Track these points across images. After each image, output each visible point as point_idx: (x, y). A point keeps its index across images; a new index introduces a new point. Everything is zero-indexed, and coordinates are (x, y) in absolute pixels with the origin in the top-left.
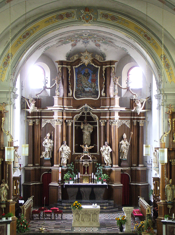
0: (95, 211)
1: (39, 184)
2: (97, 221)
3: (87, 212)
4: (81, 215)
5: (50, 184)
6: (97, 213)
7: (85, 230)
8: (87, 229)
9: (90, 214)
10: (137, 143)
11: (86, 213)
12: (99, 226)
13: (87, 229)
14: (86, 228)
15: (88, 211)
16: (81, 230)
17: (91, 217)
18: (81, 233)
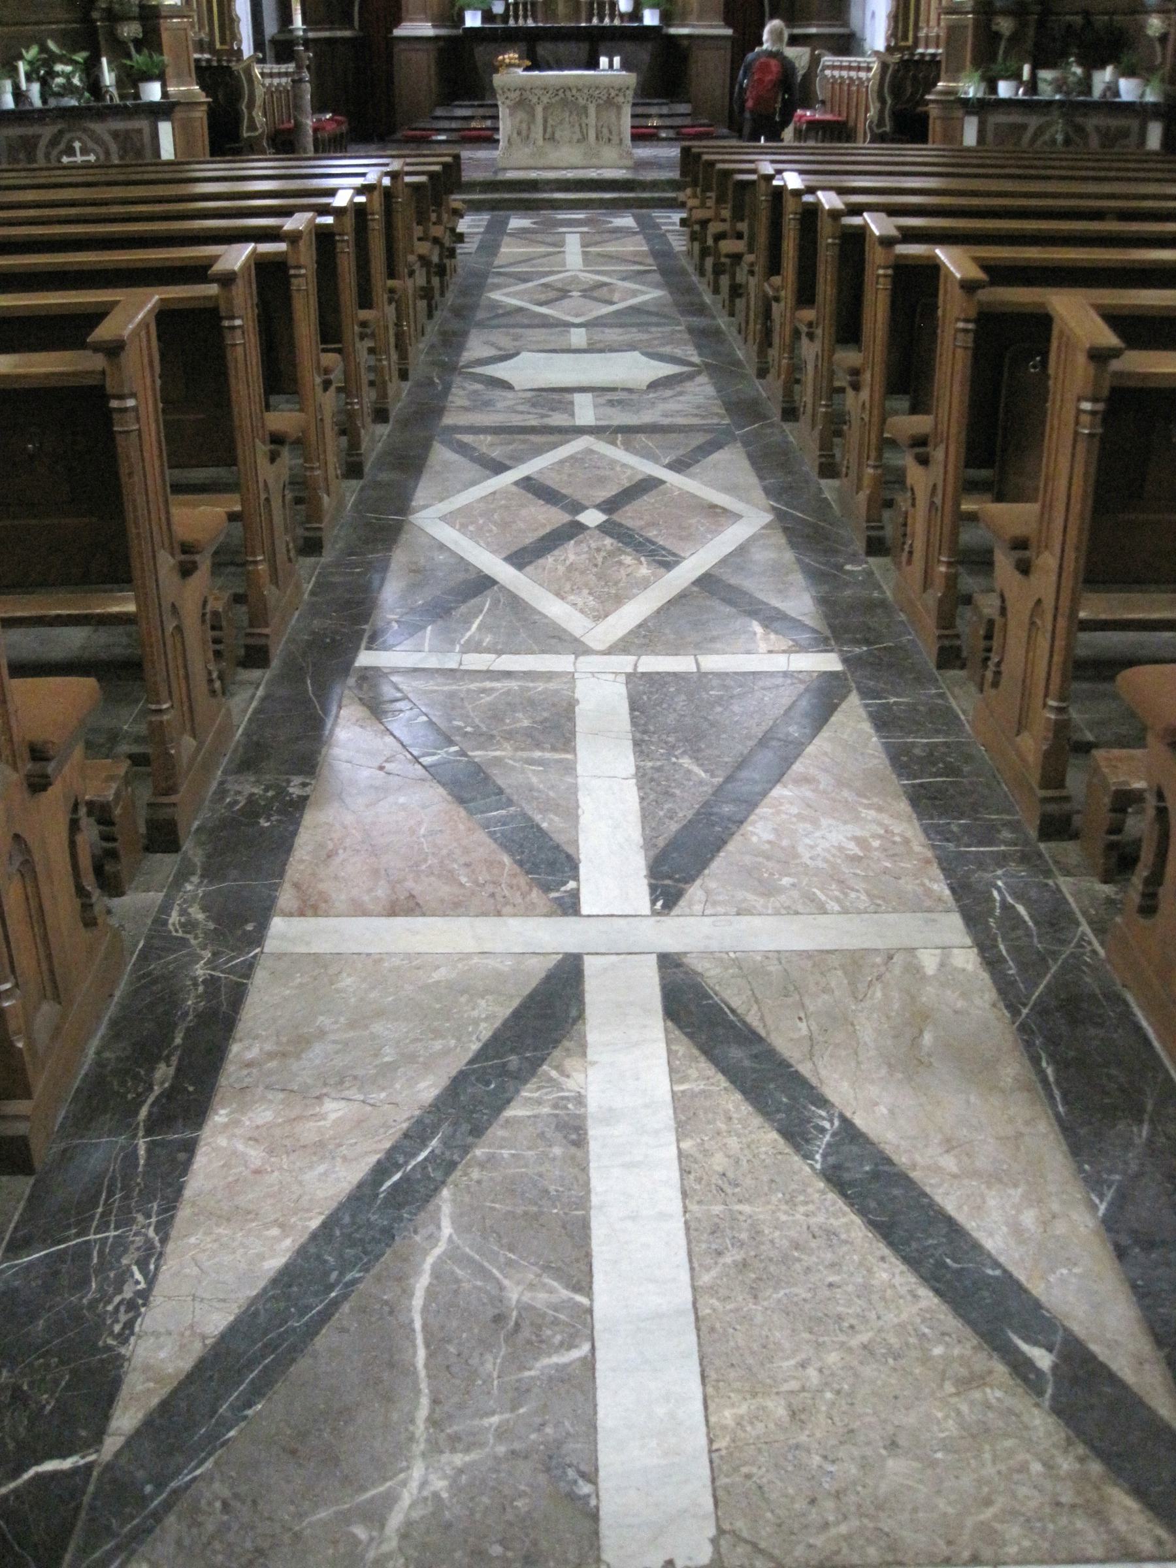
1: (344, 40)
3: (568, 93)
4: (539, 110)
5: (398, 32)
6: (621, 99)
9: (585, 108)
11: (564, 103)
17: (592, 119)
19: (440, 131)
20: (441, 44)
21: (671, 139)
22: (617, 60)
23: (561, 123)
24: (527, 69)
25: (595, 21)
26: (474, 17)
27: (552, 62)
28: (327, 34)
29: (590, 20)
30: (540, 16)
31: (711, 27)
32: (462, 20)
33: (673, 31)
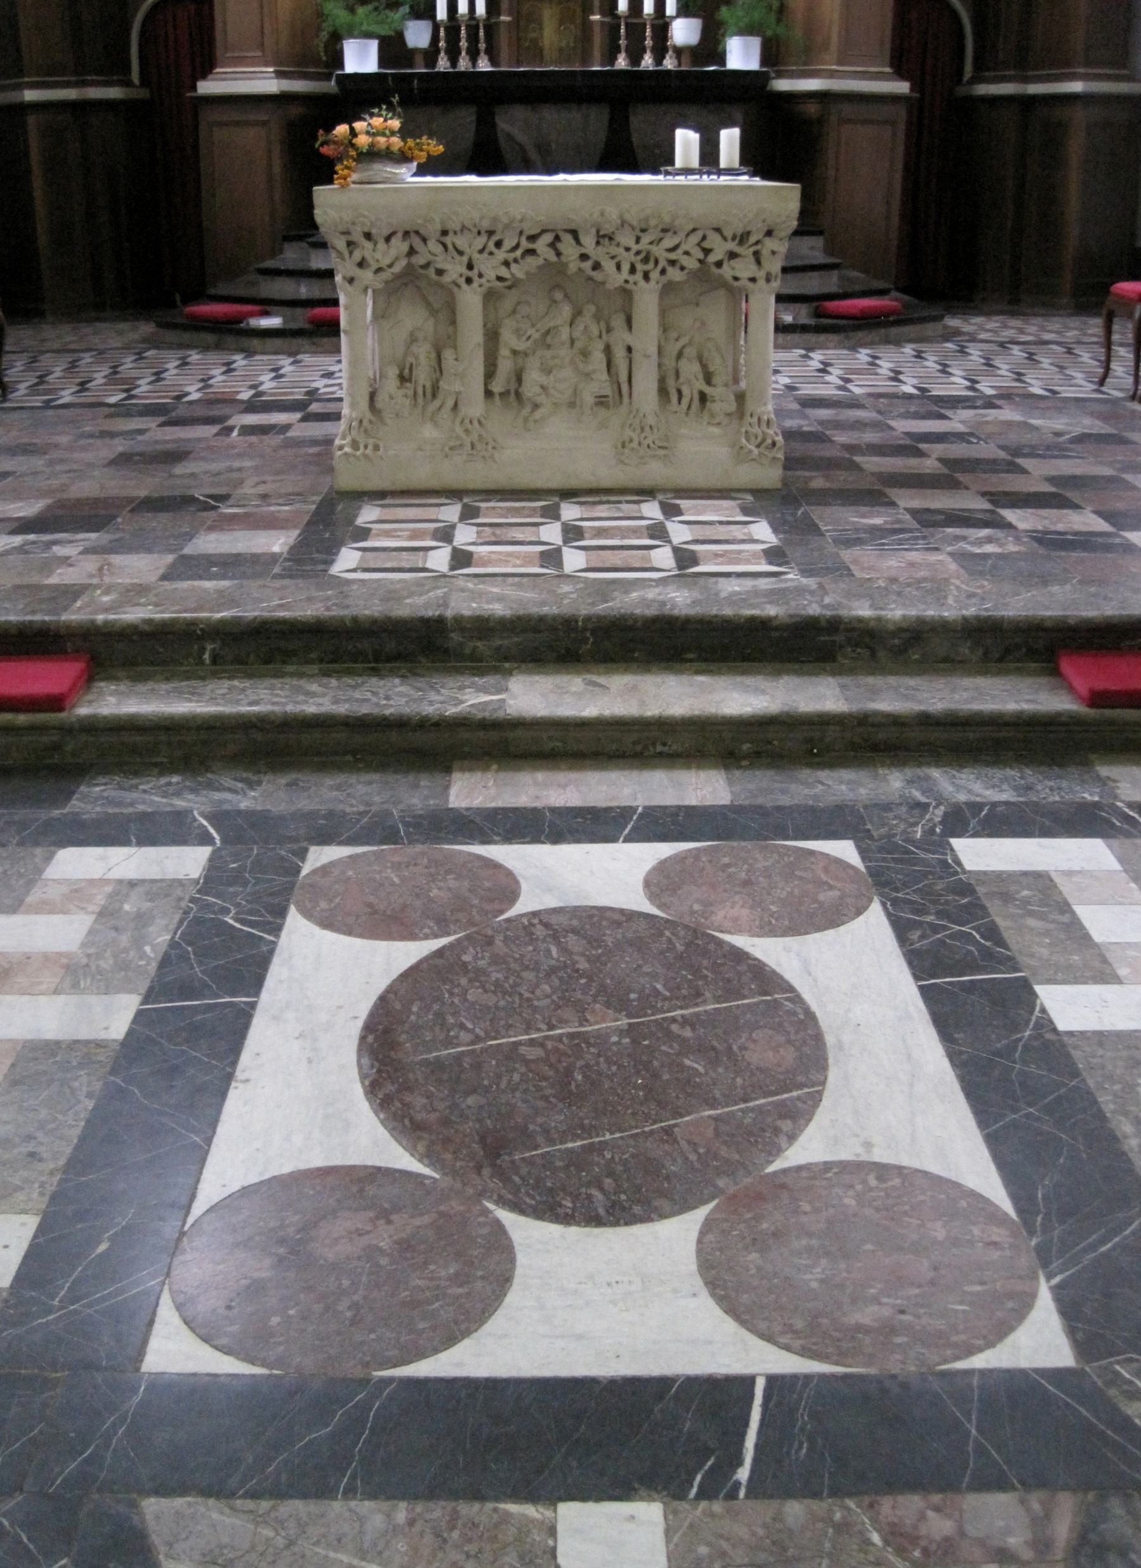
0: (714, 241)
2: (741, 398)
3: (568, 247)
4: (471, 301)
5: (207, 87)
6: (744, 268)
7: (552, 557)
8: (572, 533)
9: (626, 294)
10: (530, 500)
12: (1095, 326)
13: (572, 533)
14: (570, 512)
15: (588, 241)
16: (461, 559)
18: (460, 622)
19: (267, 306)
20: (296, 111)
21: (804, 329)
22: (730, 139)
23: (546, 340)
24: (427, 168)
25: (622, 63)
26: (362, 55)
27: (534, 156)
28: (70, 94)
29: (611, 56)
30: (504, 52)
31: (864, 76)
32: (337, 60)
33: (783, 85)
